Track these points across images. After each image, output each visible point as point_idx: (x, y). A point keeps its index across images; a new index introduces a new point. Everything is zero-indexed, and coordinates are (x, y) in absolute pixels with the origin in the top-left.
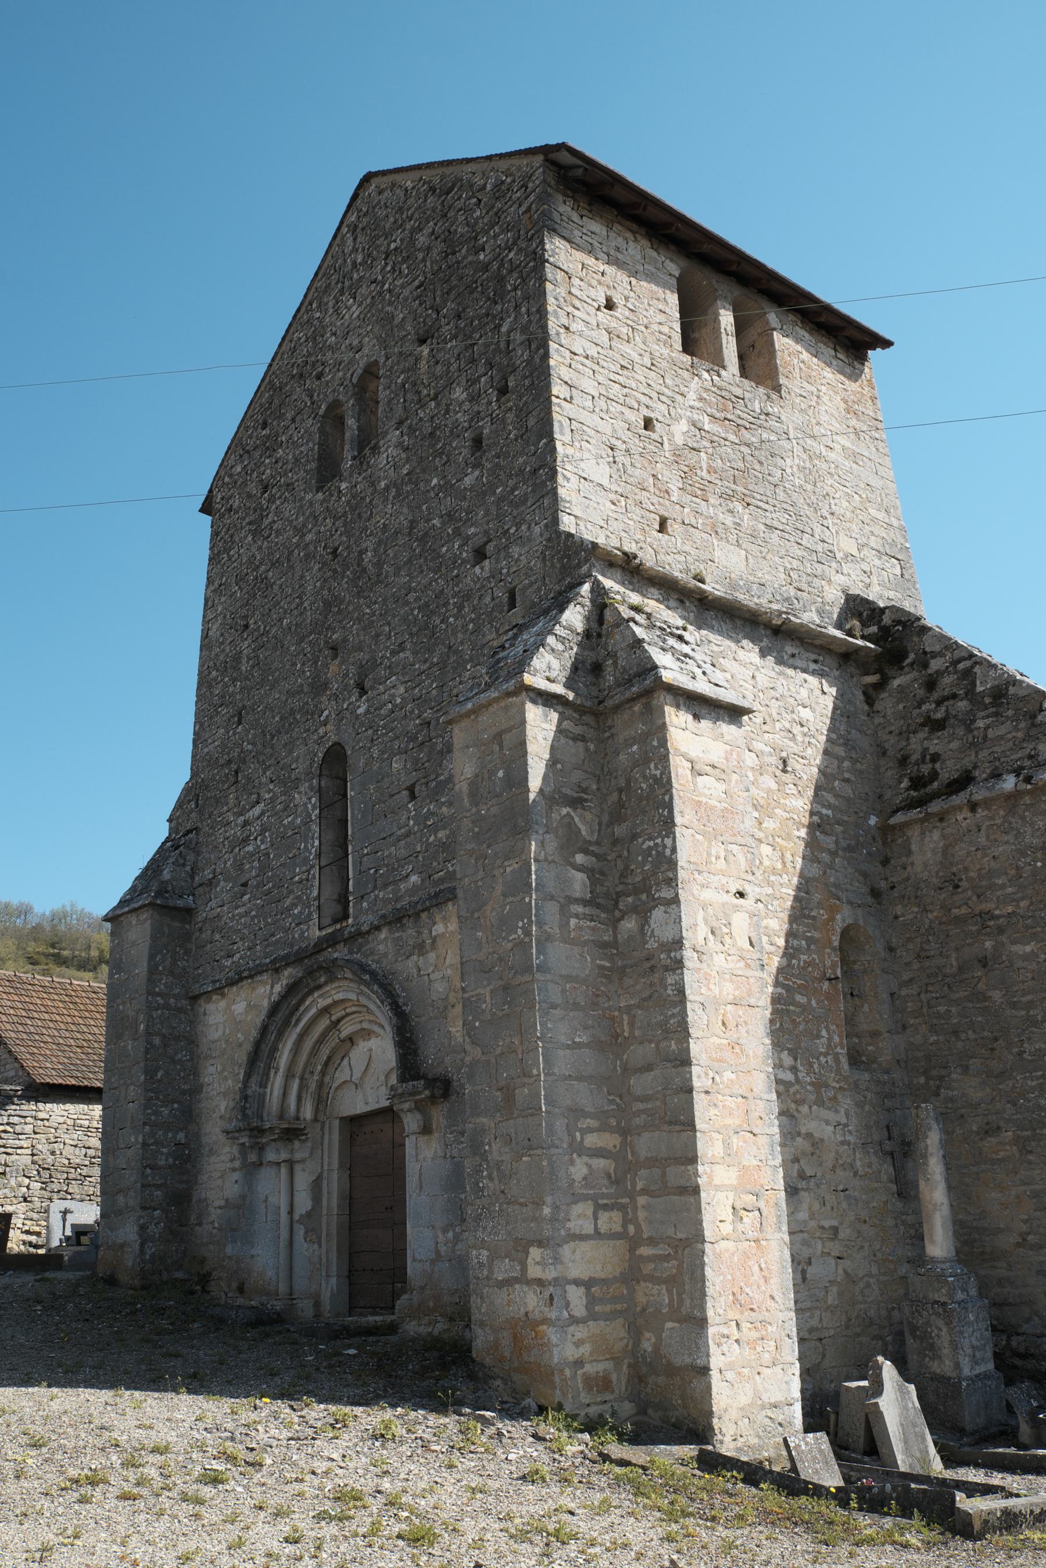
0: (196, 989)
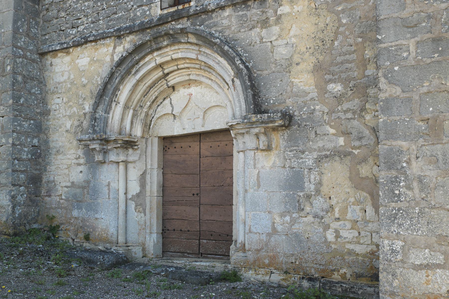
0: (45, 48)
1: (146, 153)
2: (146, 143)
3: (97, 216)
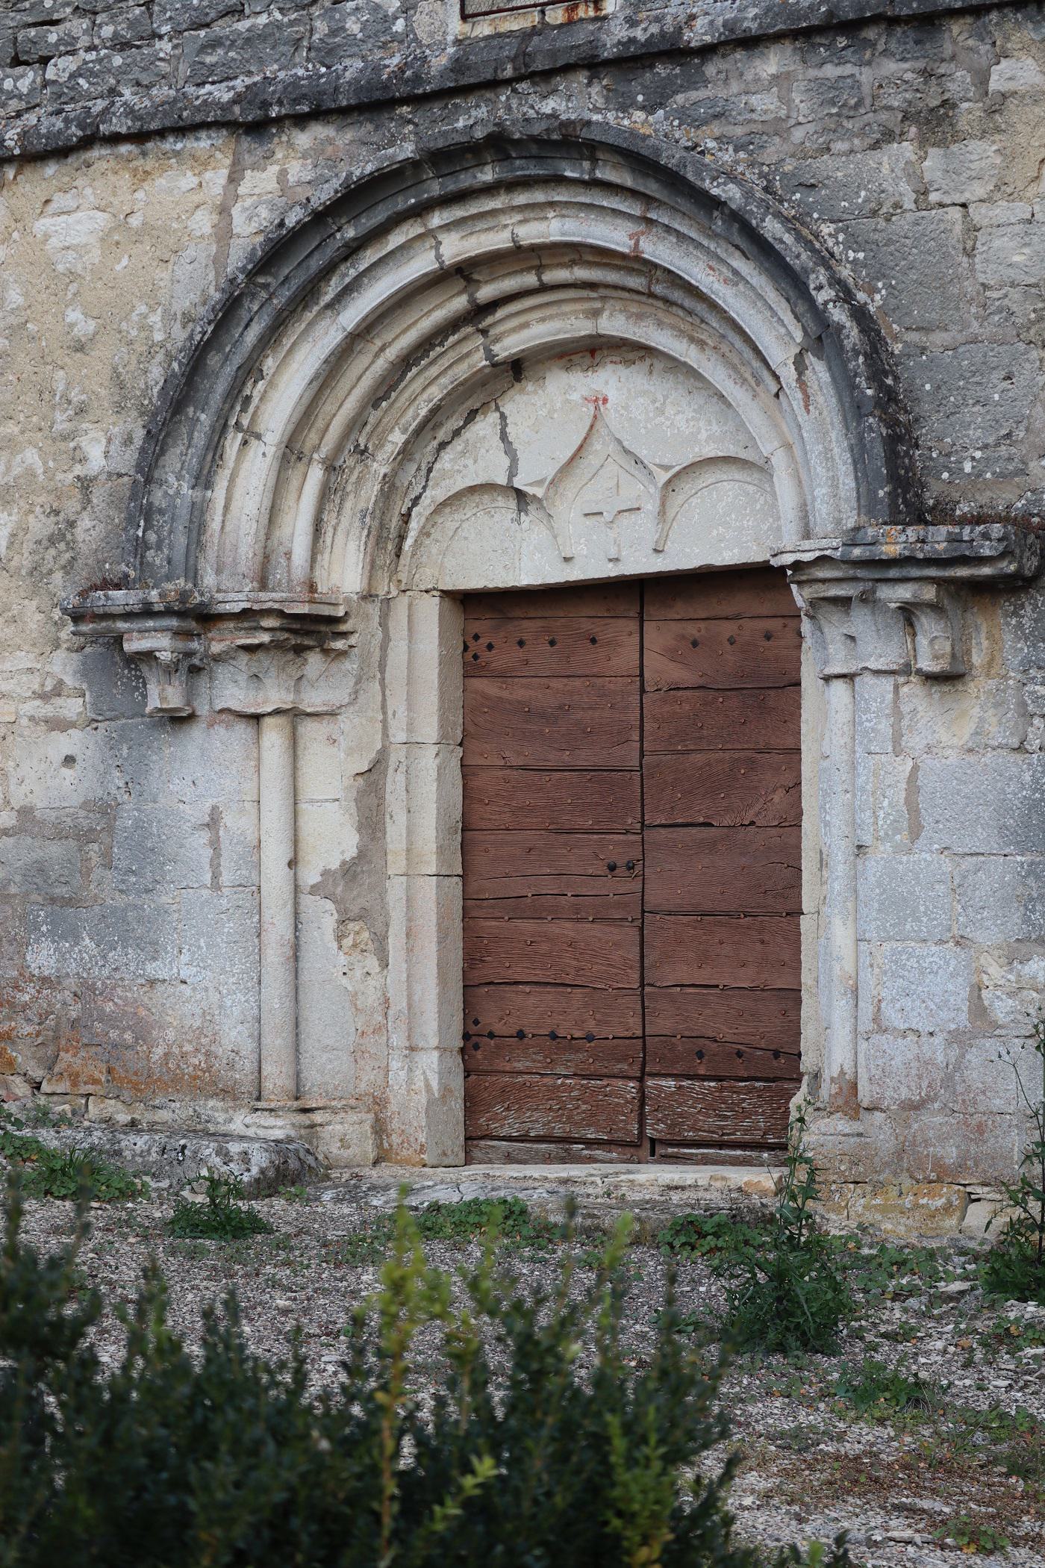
1: (382, 671)
2: (384, 624)
3: (151, 969)
